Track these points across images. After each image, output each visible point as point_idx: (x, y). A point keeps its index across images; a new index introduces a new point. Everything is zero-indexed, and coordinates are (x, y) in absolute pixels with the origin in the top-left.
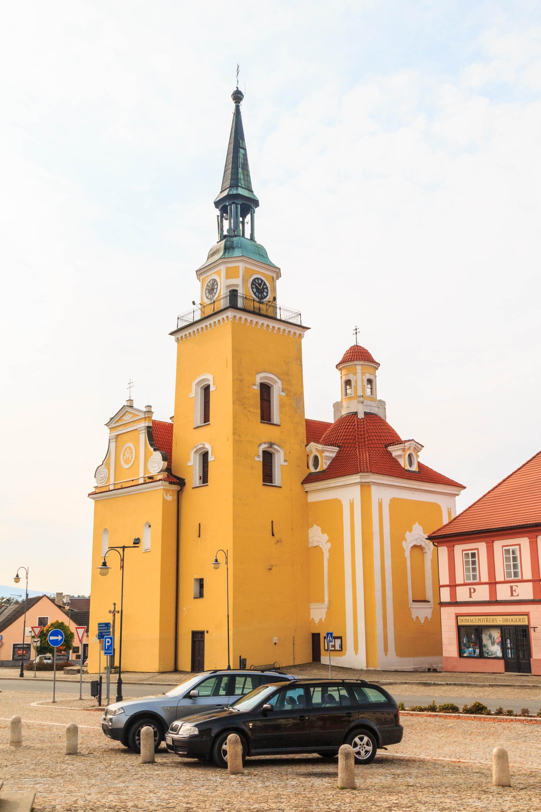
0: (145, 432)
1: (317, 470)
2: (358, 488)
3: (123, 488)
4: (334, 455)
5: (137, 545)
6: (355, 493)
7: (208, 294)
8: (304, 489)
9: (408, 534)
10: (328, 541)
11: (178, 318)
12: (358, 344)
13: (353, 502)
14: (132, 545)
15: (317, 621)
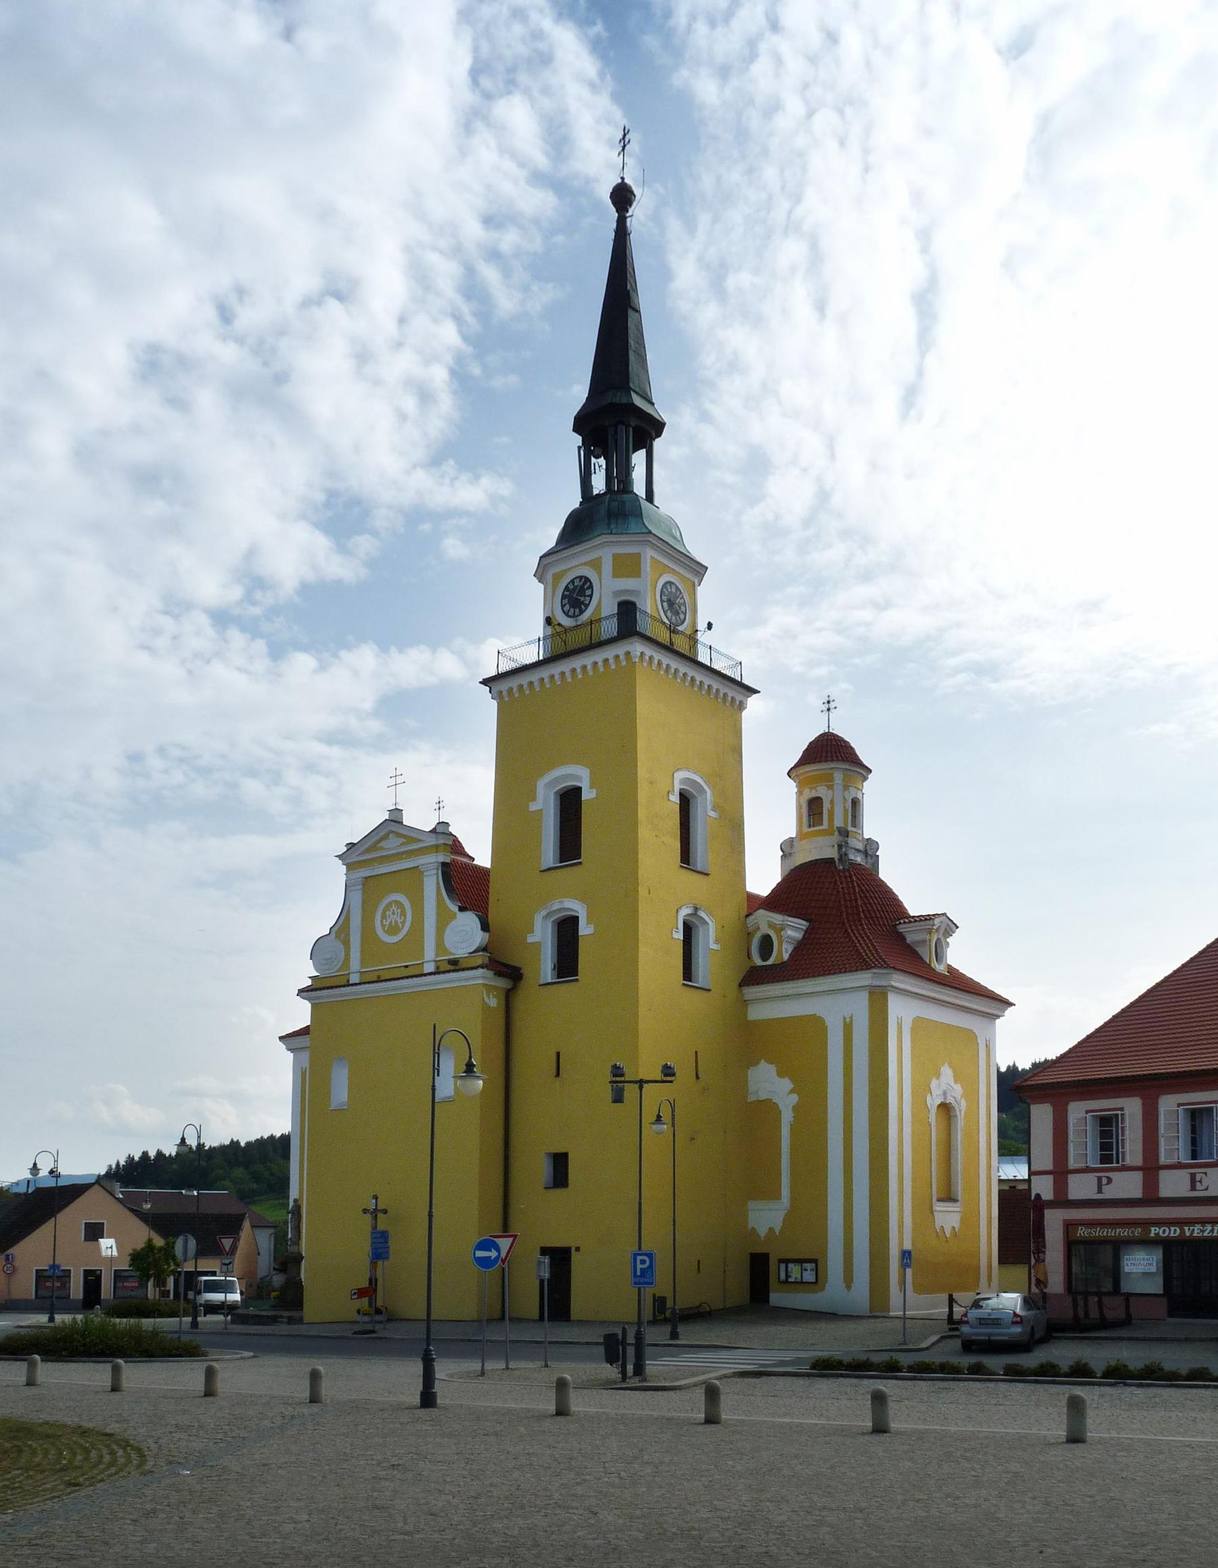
0: (437, 874)
1: (770, 962)
2: (865, 995)
3: (382, 981)
4: (798, 935)
5: (669, 1079)
6: (858, 1007)
7: (568, 605)
8: (743, 995)
9: (934, 1083)
10: (792, 1091)
11: (499, 652)
12: (831, 731)
13: (851, 1021)
14: (659, 1077)
15: (762, 1232)
